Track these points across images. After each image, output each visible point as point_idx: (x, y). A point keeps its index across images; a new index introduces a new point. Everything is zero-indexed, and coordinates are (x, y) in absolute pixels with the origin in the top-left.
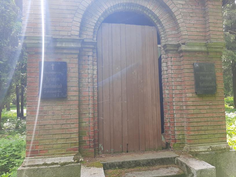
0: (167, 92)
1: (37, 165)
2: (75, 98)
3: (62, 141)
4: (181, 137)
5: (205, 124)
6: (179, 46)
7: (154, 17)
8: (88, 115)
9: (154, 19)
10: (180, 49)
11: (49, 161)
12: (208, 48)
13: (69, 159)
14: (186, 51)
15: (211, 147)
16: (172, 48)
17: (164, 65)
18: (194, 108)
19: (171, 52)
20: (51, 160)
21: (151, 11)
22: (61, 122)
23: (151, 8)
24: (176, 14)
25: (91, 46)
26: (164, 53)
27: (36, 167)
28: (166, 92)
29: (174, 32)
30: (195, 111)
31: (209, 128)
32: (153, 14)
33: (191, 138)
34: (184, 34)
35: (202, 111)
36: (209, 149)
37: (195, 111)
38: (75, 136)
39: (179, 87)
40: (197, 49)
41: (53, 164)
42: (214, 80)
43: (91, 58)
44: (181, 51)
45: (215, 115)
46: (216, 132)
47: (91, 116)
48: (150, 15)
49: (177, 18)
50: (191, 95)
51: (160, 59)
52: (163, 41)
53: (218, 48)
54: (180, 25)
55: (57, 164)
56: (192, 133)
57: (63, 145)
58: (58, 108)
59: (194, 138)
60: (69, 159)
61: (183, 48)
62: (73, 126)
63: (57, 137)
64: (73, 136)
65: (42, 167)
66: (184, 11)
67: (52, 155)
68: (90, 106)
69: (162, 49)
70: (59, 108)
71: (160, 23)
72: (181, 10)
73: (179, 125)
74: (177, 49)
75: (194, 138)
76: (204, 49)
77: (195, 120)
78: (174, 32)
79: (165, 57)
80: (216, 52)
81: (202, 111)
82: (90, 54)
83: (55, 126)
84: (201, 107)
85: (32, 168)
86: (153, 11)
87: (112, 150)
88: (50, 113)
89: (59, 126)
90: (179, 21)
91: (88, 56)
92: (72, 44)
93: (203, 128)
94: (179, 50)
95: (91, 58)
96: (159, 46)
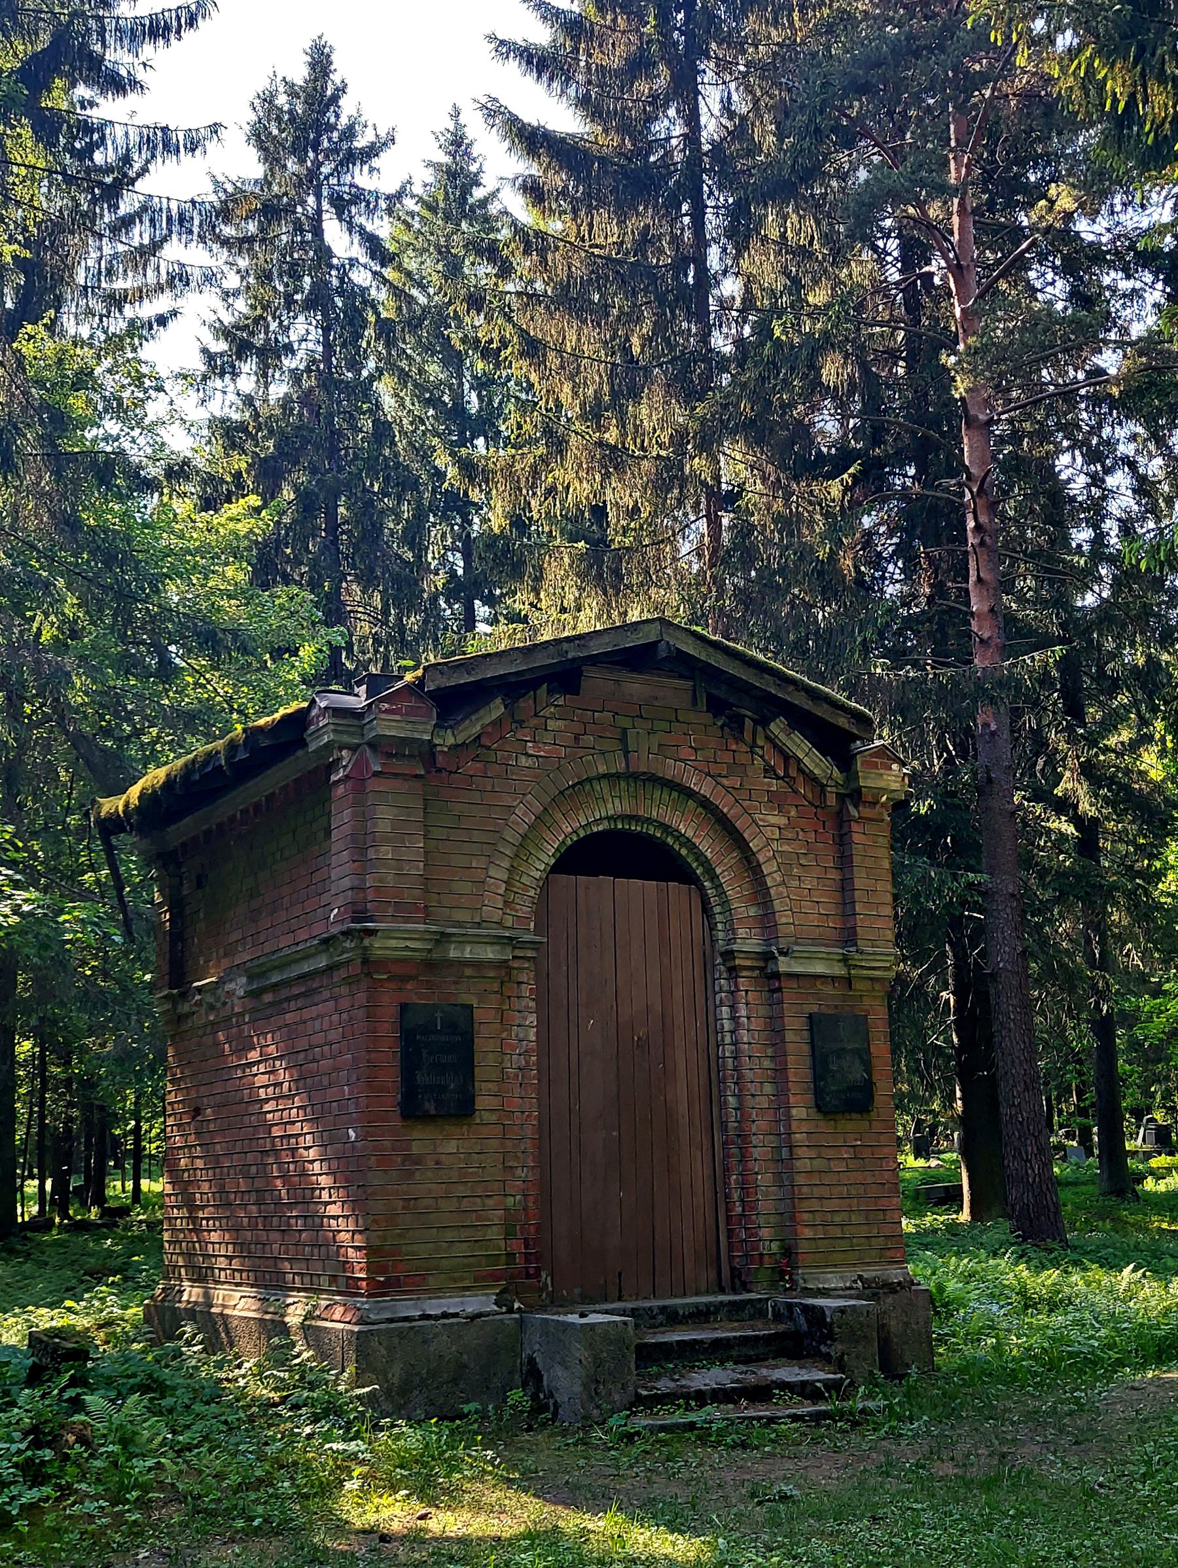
1: (406, 1319)
2: (493, 1118)
3: (462, 1250)
7: (677, 838)
8: (519, 1171)
9: (694, 865)
11: (434, 1307)
12: (849, 967)
13: (481, 1302)
14: (791, 976)
15: (860, 1277)
16: (748, 963)
19: (744, 973)
20: (439, 1306)
21: (689, 840)
22: (461, 1191)
23: (690, 834)
24: (761, 858)
25: (530, 954)
26: (725, 975)
27: (407, 1324)
30: (818, 1164)
31: (855, 1219)
32: (692, 847)
34: (784, 920)
36: (855, 1282)
37: (816, 1162)
40: (819, 968)
41: (445, 1315)
42: (1079, 1256)
43: (525, 990)
46: (875, 1232)
48: (684, 852)
53: (879, 968)
54: (772, 891)
55: (456, 1315)
57: (465, 1261)
58: (449, 1144)
60: (481, 1302)
62: (490, 1202)
63: (450, 1235)
65: (420, 1323)
66: (786, 848)
67: (437, 1292)
68: (527, 1145)
70: (452, 1146)
71: (714, 877)
72: (774, 845)
74: (762, 964)
76: (838, 970)
77: (817, 1192)
79: (726, 988)
80: (872, 979)
83: (442, 1204)
84: (831, 1153)
86: (696, 841)
87: (577, 1291)
89: (453, 1205)
91: (520, 983)
92: (489, 949)
93: (838, 1219)
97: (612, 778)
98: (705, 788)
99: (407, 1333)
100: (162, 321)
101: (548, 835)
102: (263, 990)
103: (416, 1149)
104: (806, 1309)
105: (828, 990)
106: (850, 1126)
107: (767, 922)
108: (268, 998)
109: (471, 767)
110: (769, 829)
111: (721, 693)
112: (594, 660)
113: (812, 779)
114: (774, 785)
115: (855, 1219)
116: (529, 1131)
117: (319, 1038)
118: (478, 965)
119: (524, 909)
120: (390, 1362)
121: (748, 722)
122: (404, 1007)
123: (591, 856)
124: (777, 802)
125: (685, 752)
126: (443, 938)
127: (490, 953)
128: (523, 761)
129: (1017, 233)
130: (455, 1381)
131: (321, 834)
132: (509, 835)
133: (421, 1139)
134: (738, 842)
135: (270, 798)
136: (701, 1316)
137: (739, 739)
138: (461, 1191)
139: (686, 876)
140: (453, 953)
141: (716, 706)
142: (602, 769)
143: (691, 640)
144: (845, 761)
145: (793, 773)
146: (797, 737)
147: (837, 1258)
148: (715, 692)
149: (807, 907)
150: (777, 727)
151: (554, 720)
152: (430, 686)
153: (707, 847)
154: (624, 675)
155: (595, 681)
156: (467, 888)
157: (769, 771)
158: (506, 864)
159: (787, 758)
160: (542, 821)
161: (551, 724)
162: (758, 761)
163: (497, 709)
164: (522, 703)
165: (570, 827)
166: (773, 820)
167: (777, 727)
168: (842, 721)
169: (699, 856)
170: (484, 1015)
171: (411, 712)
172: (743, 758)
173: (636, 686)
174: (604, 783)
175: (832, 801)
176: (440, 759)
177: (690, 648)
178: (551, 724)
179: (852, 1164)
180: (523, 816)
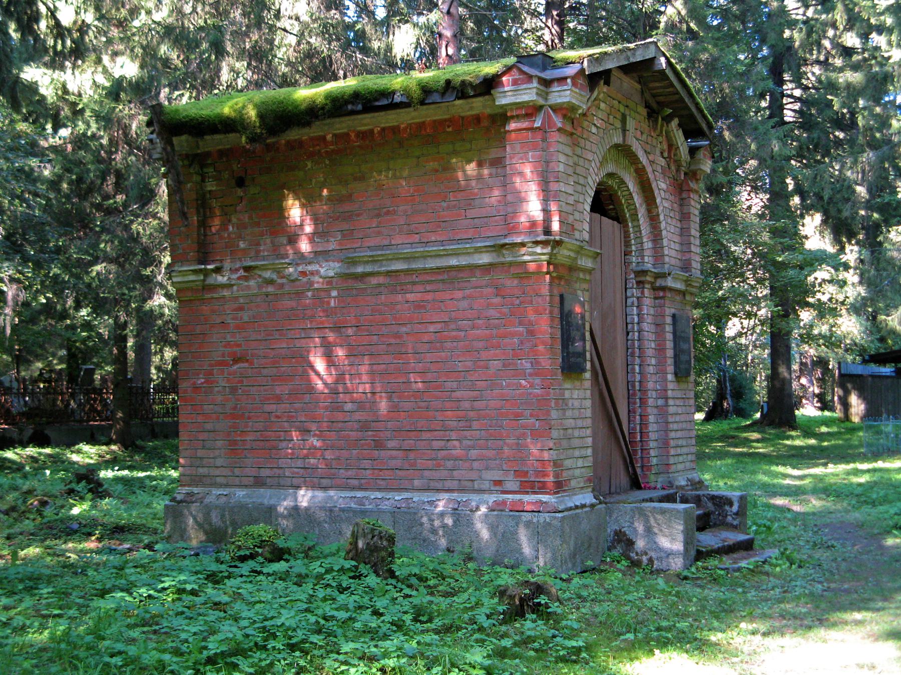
6: (658, 276)
44: (664, 289)
69: (632, 276)
85: (570, 513)
94: (658, 285)
107: (658, 256)
139: (618, 218)
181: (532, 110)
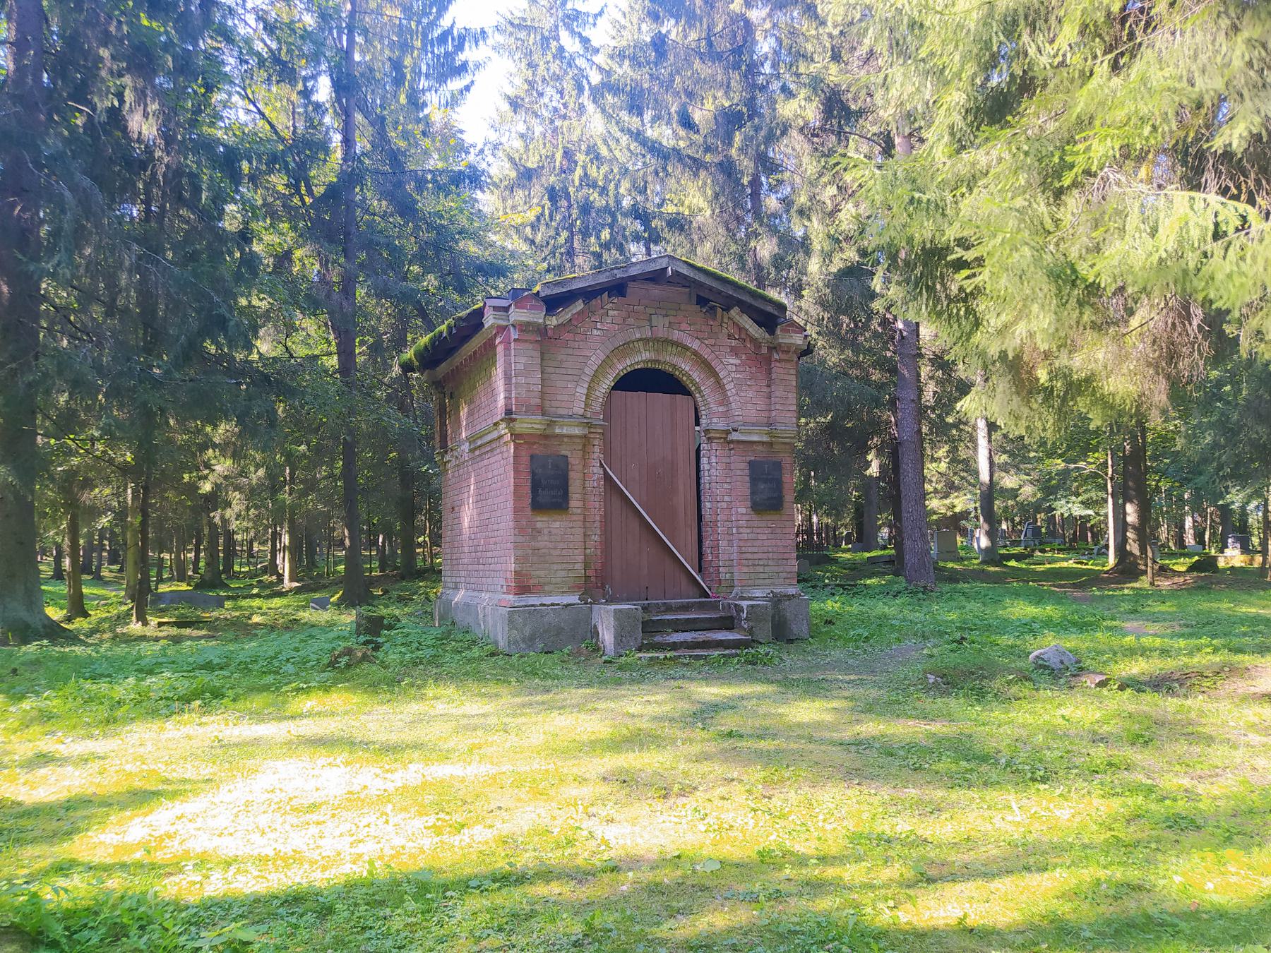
0: (708, 505)
2: (579, 511)
3: (563, 573)
4: (728, 576)
5: (765, 556)
6: (728, 432)
10: (730, 437)
11: (547, 600)
13: (574, 599)
14: (738, 442)
17: (704, 461)
18: (748, 531)
22: (561, 545)
28: (707, 505)
29: (721, 409)
31: (770, 563)
33: (743, 576)
35: (761, 537)
38: (579, 566)
39: (726, 499)
40: (755, 438)
41: (553, 605)
43: (597, 449)
44: (732, 442)
45: (779, 543)
47: (597, 538)
49: (727, 387)
50: (744, 511)
51: (698, 451)
52: (703, 421)
56: (745, 569)
58: (552, 525)
59: (747, 576)
60: (574, 599)
61: (734, 436)
63: (555, 567)
64: (577, 566)
67: (549, 594)
70: (557, 525)
71: (698, 388)
73: (726, 557)
75: (747, 576)
76: (765, 439)
78: (721, 409)
81: (761, 537)
82: (596, 442)
83: (553, 552)
84: (758, 531)
88: (546, 531)
89: (558, 552)
90: (729, 393)
93: (761, 563)
95: (597, 449)
96: (697, 428)
97: (645, 341)
98: (695, 345)
99: (531, 611)
100: (467, 88)
101: (604, 377)
102: (475, 449)
103: (539, 525)
104: (736, 605)
105: (760, 448)
106: (769, 517)
107: (727, 414)
108: (477, 453)
109: (566, 336)
110: (729, 366)
111: (705, 294)
112: (634, 278)
113: (753, 340)
114: (734, 343)
115: (770, 563)
116: (598, 518)
117: (496, 473)
118: (570, 437)
119: (597, 407)
120: (525, 625)
121: (719, 310)
122: (532, 457)
123: (634, 381)
124: (735, 351)
125: (684, 326)
126: (551, 424)
127: (577, 431)
128: (595, 332)
129: (690, 65)
130: (557, 635)
131: (278, 366)
132: (587, 370)
133: (542, 521)
134: (715, 374)
135: (475, 353)
136: (685, 608)
137: (714, 319)
138: (561, 545)
140: (557, 431)
141: (702, 301)
142: (638, 336)
143: (685, 266)
144: (771, 332)
145: (743, 336)
146: (745, 317)
147: (761, 582)
148: (701, 294)
149: (749, 406)
150: (735, 312)
151: (612, 310)
152: (542, 294)
153: (696, 376)
154: (650, 286)
155: (633, 288)
156: (565, 398)
157: (730, 336)
158: (586, 385)
159: (741, 329)
160: (606, 364)
161: (611, 313)
162: (725, 331)
163: (579, 305)
164: (594, 302)
165: (622, 366)
166: (731, 361)
167: (735, 312)
168: (769, 309)
169: (692, 381)
170: (575, 461)
171: (532, 308)
172: (716, 329)
173: (656, 291)
174: (641, 344)
175: (764, 350)
176: (550, 332)
177: (685, 270)
178: (611, 313)
179: (770, 536)
180: (595, 361)
181: (502, 329)
